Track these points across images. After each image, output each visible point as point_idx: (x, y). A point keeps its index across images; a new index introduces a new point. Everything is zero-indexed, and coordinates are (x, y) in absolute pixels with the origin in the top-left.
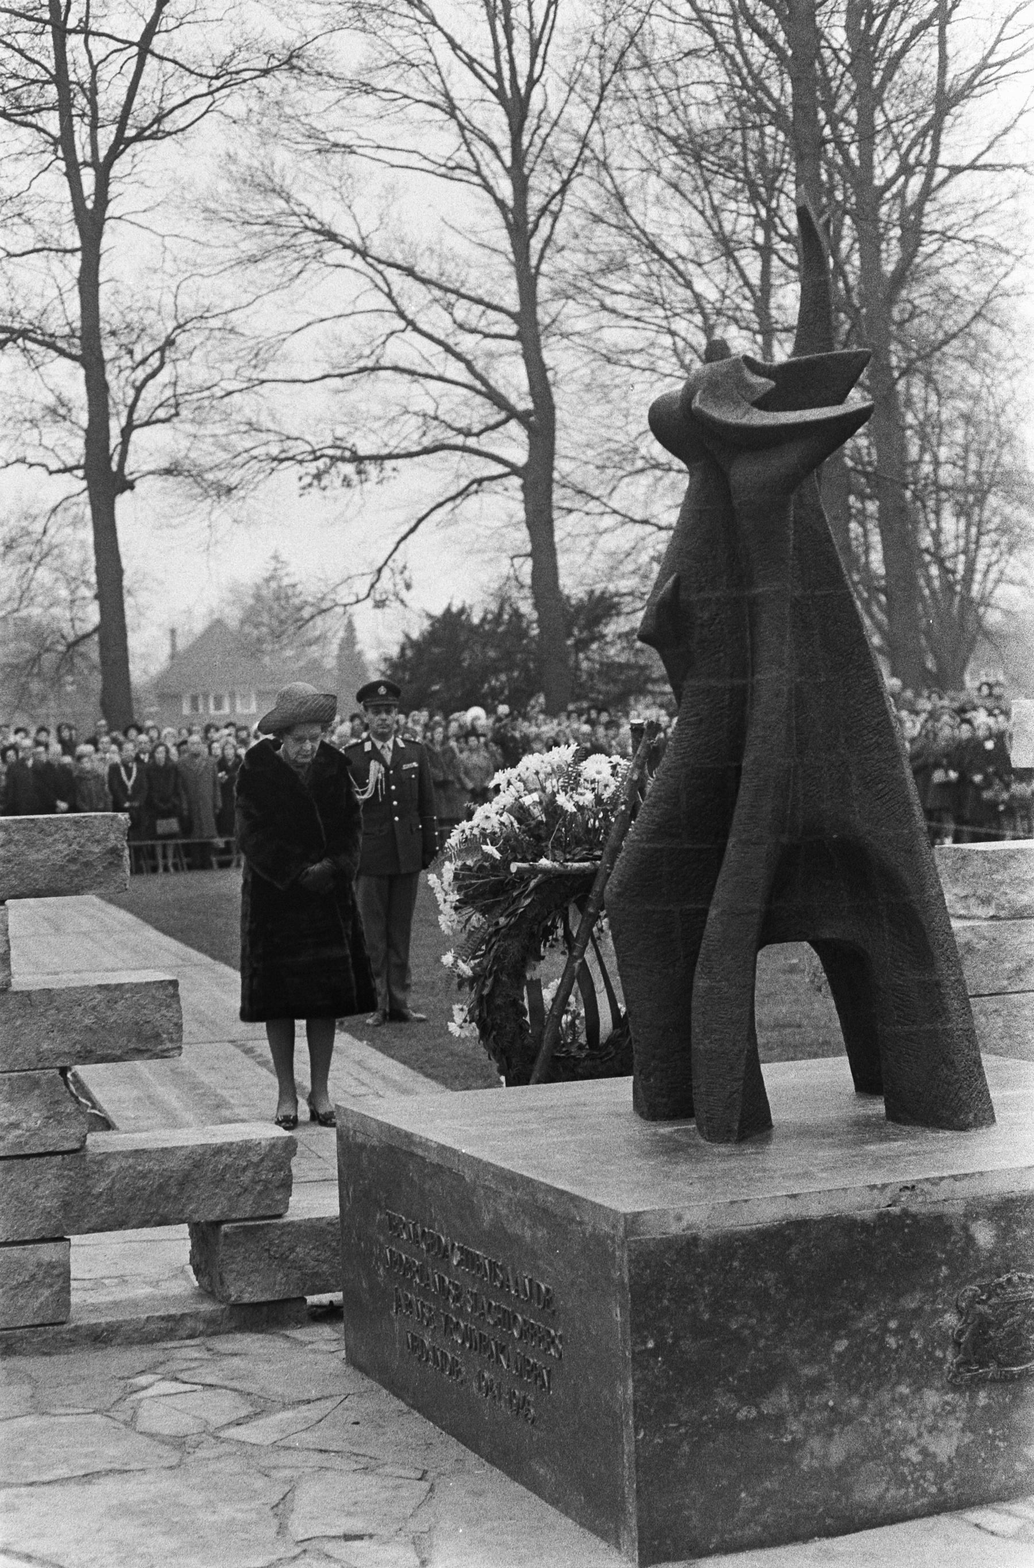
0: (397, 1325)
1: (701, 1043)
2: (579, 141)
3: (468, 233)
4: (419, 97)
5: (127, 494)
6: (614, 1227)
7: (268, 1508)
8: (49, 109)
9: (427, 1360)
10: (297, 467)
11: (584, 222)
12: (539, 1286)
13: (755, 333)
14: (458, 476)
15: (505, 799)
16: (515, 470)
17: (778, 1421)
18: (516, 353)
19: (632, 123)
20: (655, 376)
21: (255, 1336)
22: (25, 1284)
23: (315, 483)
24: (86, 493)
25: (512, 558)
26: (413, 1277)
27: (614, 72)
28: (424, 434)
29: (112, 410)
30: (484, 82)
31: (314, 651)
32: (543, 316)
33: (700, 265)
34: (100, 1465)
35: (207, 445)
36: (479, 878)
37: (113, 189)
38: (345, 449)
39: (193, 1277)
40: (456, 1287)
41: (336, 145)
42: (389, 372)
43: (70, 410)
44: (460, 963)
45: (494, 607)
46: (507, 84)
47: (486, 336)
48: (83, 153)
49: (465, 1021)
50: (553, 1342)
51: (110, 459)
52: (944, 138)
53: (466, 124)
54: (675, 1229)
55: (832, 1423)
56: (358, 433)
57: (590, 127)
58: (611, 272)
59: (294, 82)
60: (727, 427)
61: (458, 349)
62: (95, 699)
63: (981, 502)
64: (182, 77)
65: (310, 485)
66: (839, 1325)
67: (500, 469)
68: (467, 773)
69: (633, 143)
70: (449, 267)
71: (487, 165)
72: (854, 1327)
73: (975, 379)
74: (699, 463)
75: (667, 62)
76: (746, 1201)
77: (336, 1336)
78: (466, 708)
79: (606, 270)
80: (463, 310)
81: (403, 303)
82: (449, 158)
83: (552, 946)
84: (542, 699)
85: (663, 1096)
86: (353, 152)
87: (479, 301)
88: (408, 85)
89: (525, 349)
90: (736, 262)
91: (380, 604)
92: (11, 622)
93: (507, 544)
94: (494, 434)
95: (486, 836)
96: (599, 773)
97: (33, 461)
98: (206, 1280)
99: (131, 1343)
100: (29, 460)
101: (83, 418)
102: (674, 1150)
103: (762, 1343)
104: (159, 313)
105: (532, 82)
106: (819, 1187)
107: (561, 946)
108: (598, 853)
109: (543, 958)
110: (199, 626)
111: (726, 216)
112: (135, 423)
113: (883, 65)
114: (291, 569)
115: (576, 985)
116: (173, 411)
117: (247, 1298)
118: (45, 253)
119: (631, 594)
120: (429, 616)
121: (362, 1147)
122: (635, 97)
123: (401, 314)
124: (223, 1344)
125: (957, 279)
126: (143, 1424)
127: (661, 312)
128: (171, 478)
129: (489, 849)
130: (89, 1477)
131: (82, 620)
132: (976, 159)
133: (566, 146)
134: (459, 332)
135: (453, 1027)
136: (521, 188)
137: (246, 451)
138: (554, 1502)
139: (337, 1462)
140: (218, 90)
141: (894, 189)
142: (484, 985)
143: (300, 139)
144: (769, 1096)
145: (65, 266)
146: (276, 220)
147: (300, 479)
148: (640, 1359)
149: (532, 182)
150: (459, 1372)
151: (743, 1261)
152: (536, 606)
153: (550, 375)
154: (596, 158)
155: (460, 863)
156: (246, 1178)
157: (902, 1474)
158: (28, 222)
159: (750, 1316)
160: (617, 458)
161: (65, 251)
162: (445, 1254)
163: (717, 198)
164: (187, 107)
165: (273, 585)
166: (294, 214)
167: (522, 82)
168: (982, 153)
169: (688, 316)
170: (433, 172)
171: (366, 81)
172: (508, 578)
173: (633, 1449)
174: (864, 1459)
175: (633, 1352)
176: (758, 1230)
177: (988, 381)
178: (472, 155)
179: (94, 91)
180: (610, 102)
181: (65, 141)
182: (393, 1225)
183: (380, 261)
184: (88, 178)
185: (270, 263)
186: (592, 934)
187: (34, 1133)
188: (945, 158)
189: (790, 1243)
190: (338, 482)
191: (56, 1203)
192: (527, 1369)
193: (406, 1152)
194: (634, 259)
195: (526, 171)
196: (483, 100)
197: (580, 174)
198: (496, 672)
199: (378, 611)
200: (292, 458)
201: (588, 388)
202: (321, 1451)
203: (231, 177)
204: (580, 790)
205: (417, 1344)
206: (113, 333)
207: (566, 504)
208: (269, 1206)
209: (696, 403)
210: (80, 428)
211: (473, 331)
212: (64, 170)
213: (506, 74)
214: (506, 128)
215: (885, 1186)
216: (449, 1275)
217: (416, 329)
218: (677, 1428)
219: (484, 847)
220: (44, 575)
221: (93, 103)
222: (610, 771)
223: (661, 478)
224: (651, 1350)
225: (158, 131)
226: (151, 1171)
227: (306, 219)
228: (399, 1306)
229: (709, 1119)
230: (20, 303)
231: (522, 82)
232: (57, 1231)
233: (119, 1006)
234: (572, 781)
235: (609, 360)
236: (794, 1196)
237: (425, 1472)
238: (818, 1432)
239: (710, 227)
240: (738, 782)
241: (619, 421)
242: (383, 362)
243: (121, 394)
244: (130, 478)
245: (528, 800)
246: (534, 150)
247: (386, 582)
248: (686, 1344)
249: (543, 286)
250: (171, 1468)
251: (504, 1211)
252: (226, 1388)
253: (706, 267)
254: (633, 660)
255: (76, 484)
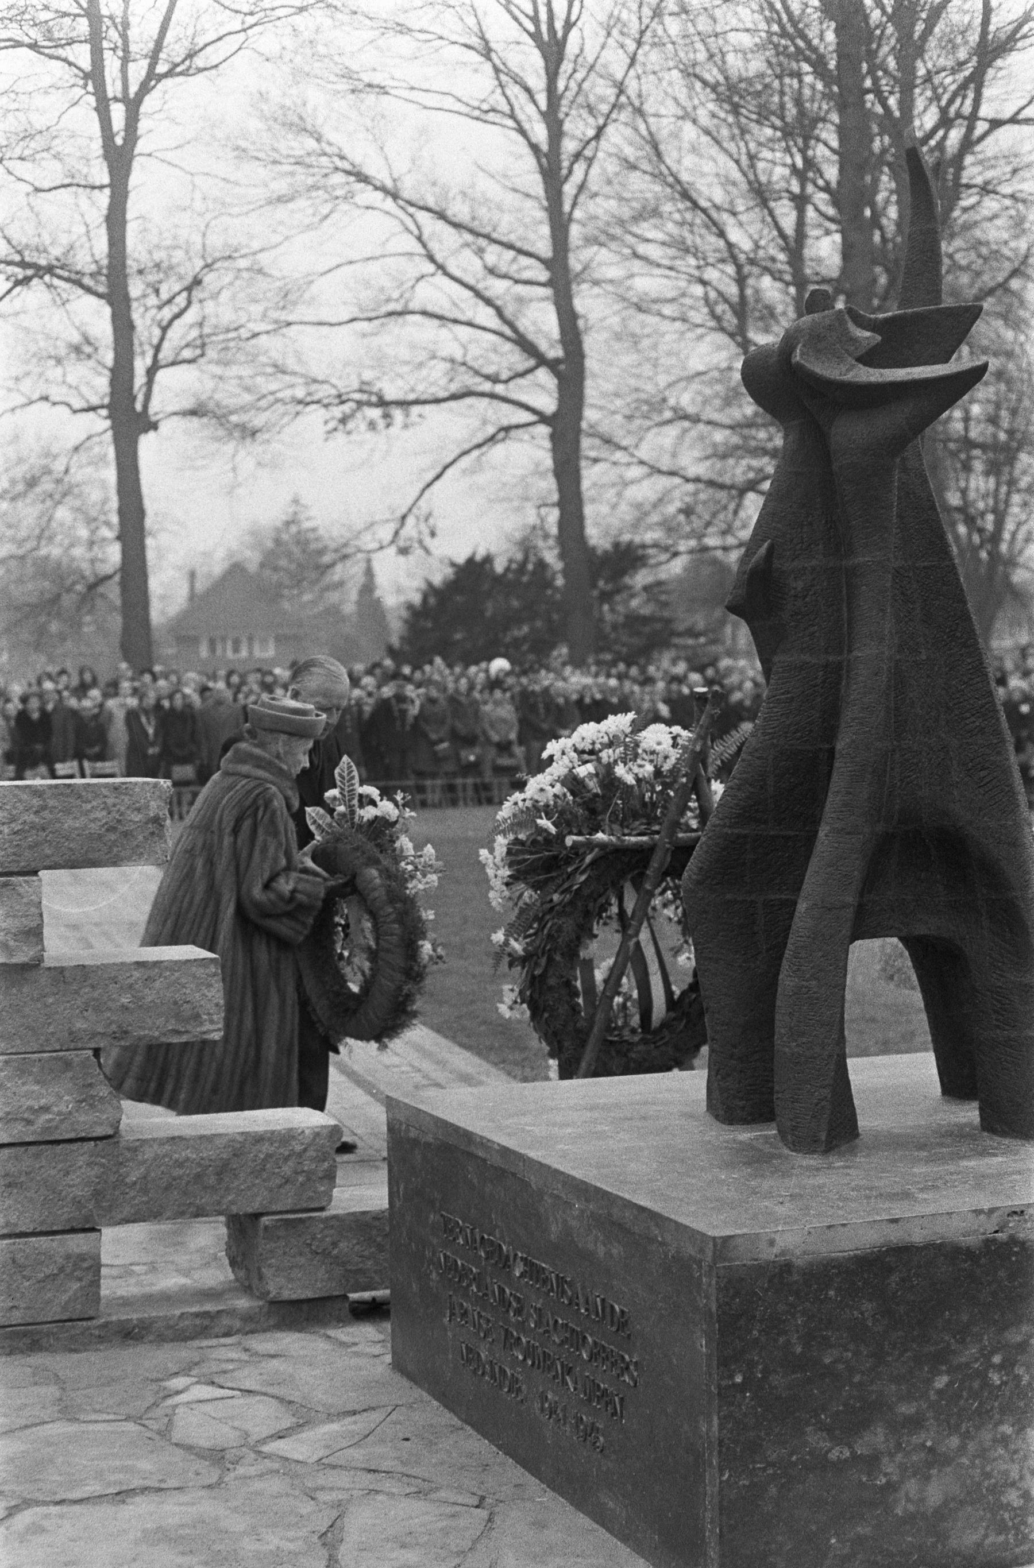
0: (449, 1334)
1: (784, 1044)
2: (615, 86)
3: (502, 177)
4: (454, 38)
5: (152, 434)
6: (701, 1251)
7: (315, 1538)
8: (81, 42)
9: (483, 1374)
10: (323, 411)
11: (618, 169)
12: (612, 1307)
13: (788, 284)
14: (485, 422)
15: (557, 769)
16: (543, 418)
17: (872, 1462)
18: (547, 298)
19: (669, 69)
20: (687, 326)
21: (297, 1335)
22: (54, 1277)
23: (341, 427)
24: (110, 433)
25: (539, 507)
26: (469, 1285)
27: (653, 18)
28: (451, 380)
29: (137, 349)
30: (520, 24)
31: (333, 597)
32: (575, 264)
33: (734, 214)
34: (136, 1483)
35: (232, 386)
36: (531, 853)
37: (143, 126)
38: (371, 393)
39: (229, 1269)
40: (518, 1300)
41: (370, 85)
42: (417, 318)
43: (96, 349)
44: (512, 942)
45: (519, 556)
46: (544, 28)
47: (517, 282)
48: (113, 88)
49: (515, 1002)
50: (627, 1368)
51: (134, 398)
52: (987, 92)
53: (502, 67)
54: (768, 1254)
55: (930, 1465)
56: (386, 378)
57: (627, 72)
58: (645, 220)
59: (329, 21)
60: (830, 383)
61: (488, 294)
62: (116, 641)
63: (1011, 460)
64: (215, 13)
65: (335, 429)
66: (940, 1359)
67: (526, 417)
68: (492, 726)
69: (669, 90)
70: (482, 212)
71: (522, 108)
72: (955, 1363)
73: (1009, 335)
74: (796, 422)
75: (706, 9)
76: (844, 1225)
77: (381, 1337)
78: (490, 659)
79: (639, 217)
80: (493, 255)
81: (434, 246)
82: (484, 101)
83: (605, 924)
84: (565, 650)
85: (741, 1099)
86: (387, 93)
87: (510, 246)
88: (443, 25)
89: (557, 294)
90: (771, 213)
91: (404, 551)
92: (29, 561)
93: (533, 492)
94: (520, 381)
95: (537, 809)
96: (659, 744)
97: (58, 399)
98: (242, 1274)
99: (164, 1341)
100: (53, 398)
101: (109, 358)
102: (758, 1161)
103: (857, 1378)
104: (187, 252)
105: (569, 25)
106: (920, 1210)
107: (615, 925)
108: (657, 828)
109: (596, 936)
110: (218, 569)
111: (761, 165)
112: (163, 363)
113: (924, 15)
114: (312, 513)
115: (629, 965)
116: (198, 352)
117: (287, 1295)
118: (74, 189)
119: (656, 545)
120: (453, 564)
121: (415, 1142)
122: (673, 43)
123: (431, 258)
124: (262, 1343)
125: (995, 233)
126: (177, 1436)
127: (692, 261)
128: (195, 420)
129: (544, 823)
130: (123, 1496)
131: (102, 561)
132: (1018, 113)
133: (602, 90)
134: (489, 277)
135: (503, 1009)
136: (556, 133)
137: (272, 393)
138: (625, 1539)
139: (388, 1485)
140: (251, 27)
141: (933, 143)
142: (536, 964)
143: (333, 78)
144: (856, 1102)
145: (93, 203)
146: (307, 160)
147: (326, 422)
148: (726, 1394)
149: (567, 126)
150: (519, 1390)
151: (839, 1290)
152: (562, 556)
153: (581, 323)
154: (631, 104)
155: (511, 837)
156: (287, 1169)
157: (1003, 1520)
158: (57, 157)
159: (847, 1350)
160: (645, 408)
161: (93, 188)
162: (506, 1263)
163: (752, 145)
164: (219, 43)
165: (294, 529)
166: (325, 154)
167: (559, 25)
168: (1023, 108)
169: (720, 266)
170: (467, 115)
171: (401, 21)
172: (534, 528)
173: (716, 1489)
174: (962, 1503)
175: (719, 1387)
176: (856, 1256)
177: (1022, 338)
178: (507, 98)
179: (126, 25)
180: (647, 48)
181: (95, 76)
182: (448, 1228)
183: (412, 205)
184: (118, 113)
185: (301, 203)
186: (646, 914)
187: (66, 1116)
188: (986, 110)
189: (890, 1270)
190: (363, 427)
191: (87, 1192)
192: (595, 1393)
193: (464, 1152)
194: (667, 208)
195: (561, 116)
196: (518, 43)
197: (615, 121)
198: (519, 622)
199: (402, 559)
200: (318, 402)
201: (618, 337)
202: (370, 1471)
203: (263, 117)
204: (639, 762)
205: (471, 1355)
206: (140, 272)
207: (593, 454)
208: (311, 1198)
209: (797, 357)
210: (105, 367)
211: (505, 276)
212: (94, 104)
213: (543, 16)
214: (542, 72)
215: (992, 1211)
216: (511, 1287)
217: (446, 274)
218: (764, 1469)
219: (539, 821)
220: (62, 514)
221: (124, 37)
222: (671, 742)
223: (685, 431)
224: (739, 1384)
225: (190, 67)
226: (187, 1159)
227: (336, 160)
228: (452, 1314)
229: (794, 1128)
230: (47, 239)
231: (559, 25)
232: (88, 1222)
233: (157, 984)
234: (632, 753)
235: (639, 309)
236: (895, 1221)
237: (482, 1498)
238: (914, 1475)
239: (745, 174)
240: (831, 766)
241: (647, 370)
242: (412, 306)
243: (146, 334)
244: (153, 419)
245: (584, 771)
246: (570, 95)
247: (410, 529)
248: (776, 1379)
249: (575, 231)
250: (210, 1487)
251: (574, 1223)
252: (265, 1394)
253: (740, 217)
254: (658, 614)
255: (100, 423)
